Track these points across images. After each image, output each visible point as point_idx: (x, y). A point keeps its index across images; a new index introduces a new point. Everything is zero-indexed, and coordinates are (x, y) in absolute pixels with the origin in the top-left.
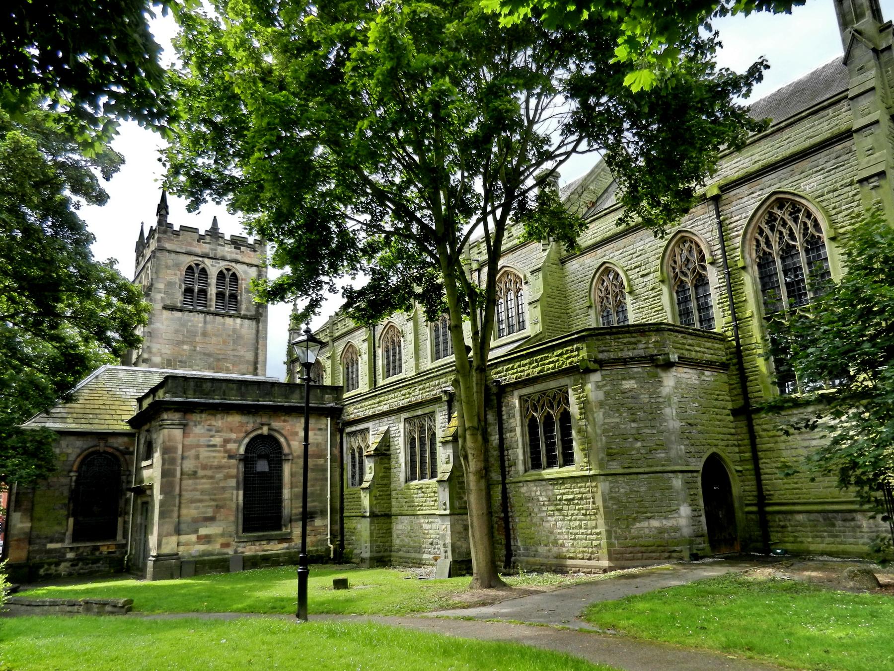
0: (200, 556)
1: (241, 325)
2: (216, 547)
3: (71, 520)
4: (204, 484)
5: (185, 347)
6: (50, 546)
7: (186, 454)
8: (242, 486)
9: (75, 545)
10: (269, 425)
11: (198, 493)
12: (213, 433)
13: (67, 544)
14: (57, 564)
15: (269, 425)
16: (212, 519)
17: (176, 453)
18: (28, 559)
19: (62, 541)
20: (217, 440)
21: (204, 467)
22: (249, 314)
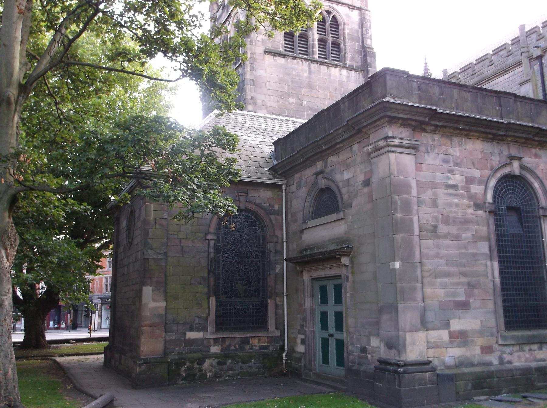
0: (456, 366)
1: (348, 77)
2: (474, 352)
3: (213, 300)
4: (448, 247)
5: (291, 100)
6: (191, 335)
7: (421, 197)
8: (495, 253)
9: (220, 335)
10: (520, 159)
11: (442, 261)
12: (451, 166)
13: (210, 334)
14: (201, 361)
15: (520, 159)
16: (464, 305)
17: (410, 193)
18: (165, 353)
19: (204, 329)
20: (457, 179)
21: (446, 221)
22: (355, 64)
